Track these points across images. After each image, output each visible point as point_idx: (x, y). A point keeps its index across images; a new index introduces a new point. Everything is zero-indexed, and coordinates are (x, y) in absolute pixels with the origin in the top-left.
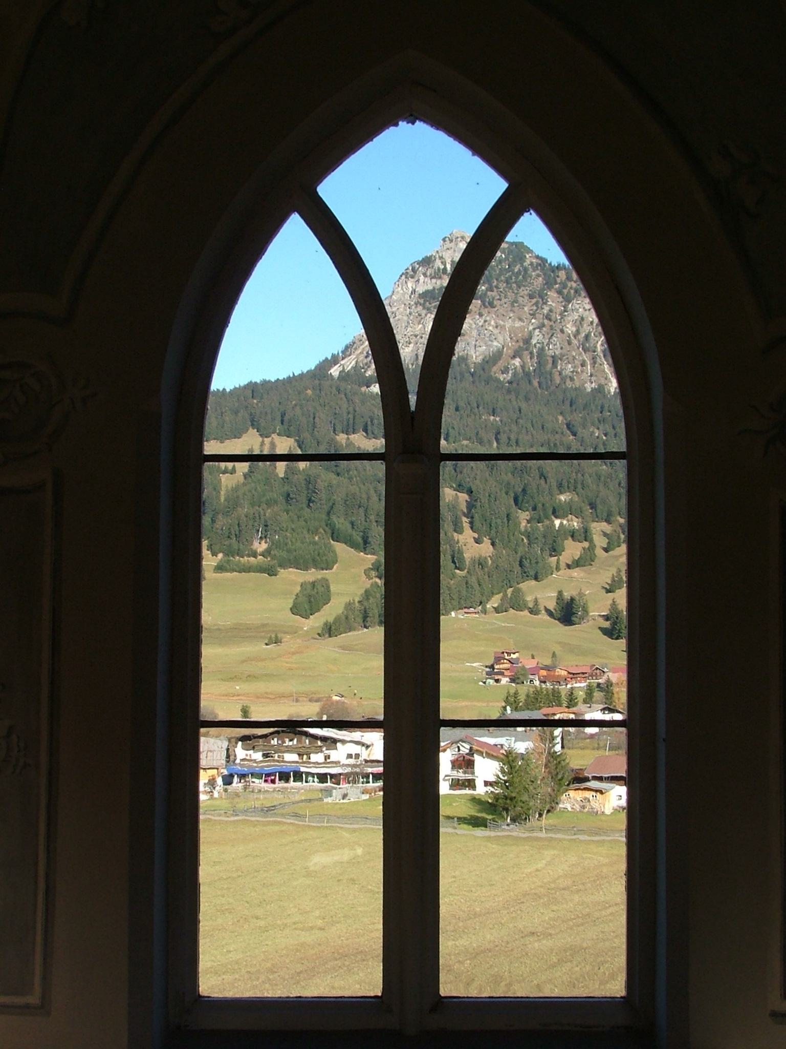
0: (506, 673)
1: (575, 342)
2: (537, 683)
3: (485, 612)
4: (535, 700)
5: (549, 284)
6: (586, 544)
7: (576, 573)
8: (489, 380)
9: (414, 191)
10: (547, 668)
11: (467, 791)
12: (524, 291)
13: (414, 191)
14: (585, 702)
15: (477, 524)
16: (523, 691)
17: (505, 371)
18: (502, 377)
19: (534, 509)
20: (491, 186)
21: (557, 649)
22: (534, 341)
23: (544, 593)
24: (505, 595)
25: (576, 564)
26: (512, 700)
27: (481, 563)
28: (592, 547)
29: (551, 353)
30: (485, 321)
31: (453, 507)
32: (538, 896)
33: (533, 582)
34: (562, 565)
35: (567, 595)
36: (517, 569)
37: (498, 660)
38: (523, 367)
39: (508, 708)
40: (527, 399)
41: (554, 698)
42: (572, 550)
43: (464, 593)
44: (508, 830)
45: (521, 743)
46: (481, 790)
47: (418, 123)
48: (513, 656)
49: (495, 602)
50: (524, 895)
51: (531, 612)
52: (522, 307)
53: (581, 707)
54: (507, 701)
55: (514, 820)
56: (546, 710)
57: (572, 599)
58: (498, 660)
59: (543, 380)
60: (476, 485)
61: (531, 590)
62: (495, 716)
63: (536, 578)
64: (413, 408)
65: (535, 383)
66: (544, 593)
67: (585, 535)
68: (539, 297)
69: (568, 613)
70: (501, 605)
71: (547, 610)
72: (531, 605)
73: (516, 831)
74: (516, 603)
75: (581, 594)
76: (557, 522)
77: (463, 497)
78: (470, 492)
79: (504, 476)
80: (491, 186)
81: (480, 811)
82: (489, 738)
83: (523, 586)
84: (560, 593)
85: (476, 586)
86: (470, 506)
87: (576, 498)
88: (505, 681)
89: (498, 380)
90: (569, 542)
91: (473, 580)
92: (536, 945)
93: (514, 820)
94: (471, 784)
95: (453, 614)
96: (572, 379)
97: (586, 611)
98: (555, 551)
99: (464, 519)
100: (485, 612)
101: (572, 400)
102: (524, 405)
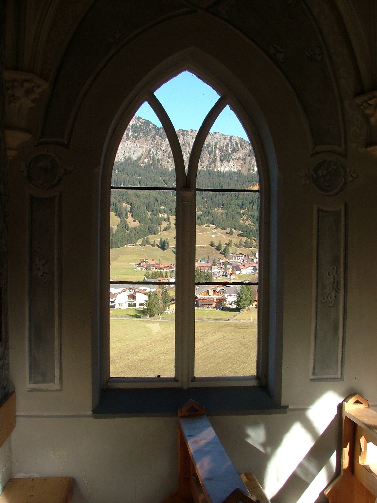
0: (144, 266)
1: (165, 154)
2: (154, 270)
3: (136, 245)
4: (155, 275)
5: (157, 133)
6: (168, 223)
7: (166, 232)
8: (138, 166)
9: (186, 98)
10: (158, 264)
11: (134, 308)
12: (149, 136)
13: (186, 98)
14: (170, 276)
15: (134, 215)
16: (150, 272)
17: (143, 163)
18: (142, 165)
19: (153, 211)
20: (214, 97)
21: (160, 258)
22: (151, 152)
23: (156, 239)
24: (144, 239)
25: (166, 229)
26: (147, 275)
27: (135, 229)
28: (170, 224)
29: (157, 158)
30: (137, 145)
31: (125, 209)
32: (161, 341)
33: (153, 235)
34: (162, 230)
35: (163, 240)
36: (147, 230)
37: (142, 261)
38: (148, 162)
39: (146, 278)
40: (149, 172)
41: (161, 275)
42: (165, 224)
43: (129, 239)
44: (148, 318)
45: (148, 289)
46: (138, 307)
47: (186, 71)
48: (146, 260)
49: (140, 242)
50: (157, 341)
51: (152, 245)
52: (148, 141)
53: (169, 278)
54: (145, 276)
55: (150, 316)
56: (160, 279)
57: (165, 241)
58: (142, 261)
59: (154, 167)
60: (134, 202)
61: (151, 238)
62: (142, 280)
63: (155, 234)
64: (186, 175)
65: (152, 168)
66: (156, 239)
67: (168, 220)
68: (154, 137)
69: (163, 246)
70: (142, 243)
71: (157, 245)
72: (152, 243)
73: (151, 319)
74: (146, 243)
75: (167, 239)
76: (160, 215)
77: (129, 206)
78: (131, 205)
79: (142, 200)
80: (214, 97)
81: (138, 313)
82: (142, 287)
83: (149, 236)
84: (161, 239)
85: (133, 237)
86: (131, 209)
87: (166, 208)
88: (144, 269)
89: (140, 166)
90: (164, 222)
91: (132, 234)
92: (163, 357)
93: (150, 316)
94: (134, 305)
95: (125, 246)
96: (164, 166)
97: (168, 246)
98: (160, 224)
99: (129, 213)
100: (136, 245)
101: (165, 173)
102: (148, 174)
